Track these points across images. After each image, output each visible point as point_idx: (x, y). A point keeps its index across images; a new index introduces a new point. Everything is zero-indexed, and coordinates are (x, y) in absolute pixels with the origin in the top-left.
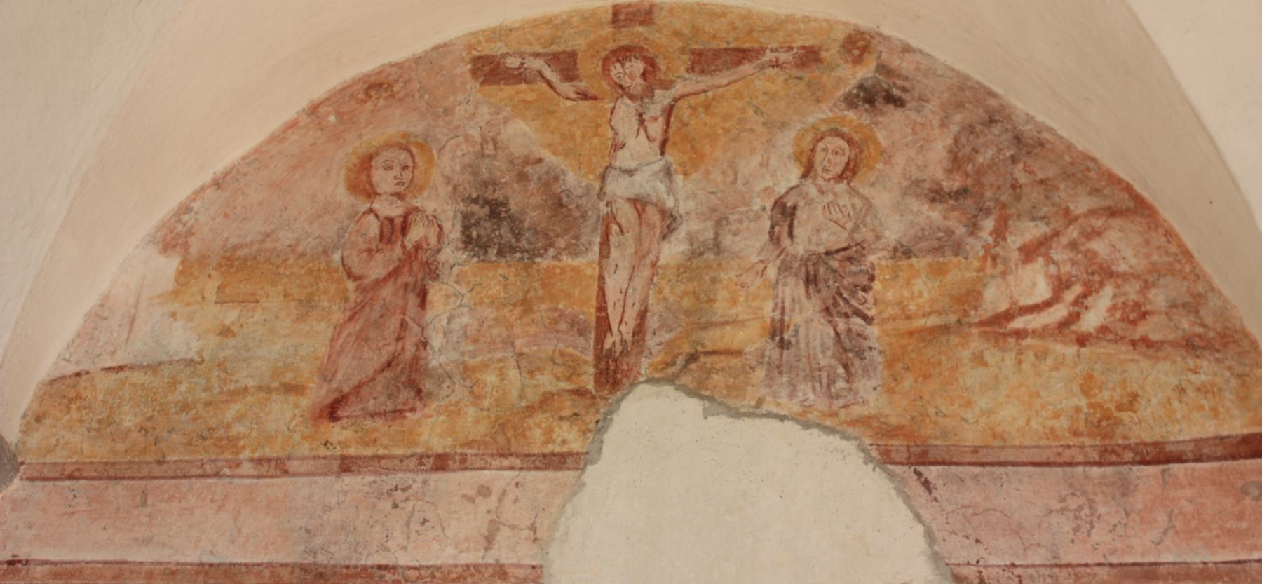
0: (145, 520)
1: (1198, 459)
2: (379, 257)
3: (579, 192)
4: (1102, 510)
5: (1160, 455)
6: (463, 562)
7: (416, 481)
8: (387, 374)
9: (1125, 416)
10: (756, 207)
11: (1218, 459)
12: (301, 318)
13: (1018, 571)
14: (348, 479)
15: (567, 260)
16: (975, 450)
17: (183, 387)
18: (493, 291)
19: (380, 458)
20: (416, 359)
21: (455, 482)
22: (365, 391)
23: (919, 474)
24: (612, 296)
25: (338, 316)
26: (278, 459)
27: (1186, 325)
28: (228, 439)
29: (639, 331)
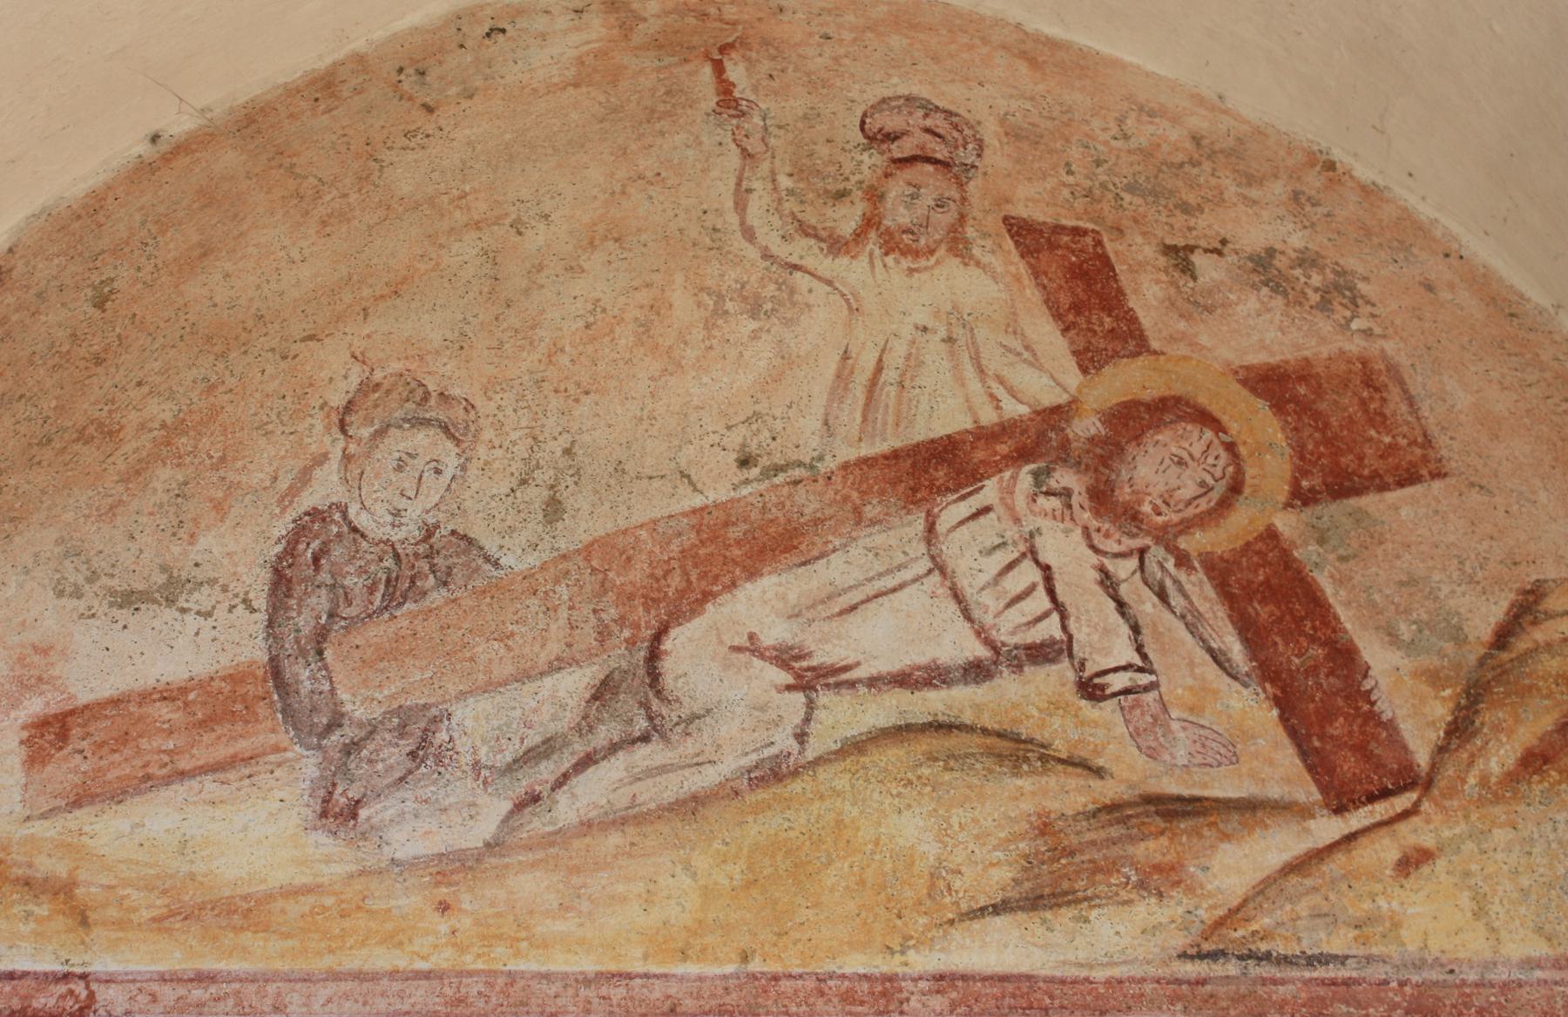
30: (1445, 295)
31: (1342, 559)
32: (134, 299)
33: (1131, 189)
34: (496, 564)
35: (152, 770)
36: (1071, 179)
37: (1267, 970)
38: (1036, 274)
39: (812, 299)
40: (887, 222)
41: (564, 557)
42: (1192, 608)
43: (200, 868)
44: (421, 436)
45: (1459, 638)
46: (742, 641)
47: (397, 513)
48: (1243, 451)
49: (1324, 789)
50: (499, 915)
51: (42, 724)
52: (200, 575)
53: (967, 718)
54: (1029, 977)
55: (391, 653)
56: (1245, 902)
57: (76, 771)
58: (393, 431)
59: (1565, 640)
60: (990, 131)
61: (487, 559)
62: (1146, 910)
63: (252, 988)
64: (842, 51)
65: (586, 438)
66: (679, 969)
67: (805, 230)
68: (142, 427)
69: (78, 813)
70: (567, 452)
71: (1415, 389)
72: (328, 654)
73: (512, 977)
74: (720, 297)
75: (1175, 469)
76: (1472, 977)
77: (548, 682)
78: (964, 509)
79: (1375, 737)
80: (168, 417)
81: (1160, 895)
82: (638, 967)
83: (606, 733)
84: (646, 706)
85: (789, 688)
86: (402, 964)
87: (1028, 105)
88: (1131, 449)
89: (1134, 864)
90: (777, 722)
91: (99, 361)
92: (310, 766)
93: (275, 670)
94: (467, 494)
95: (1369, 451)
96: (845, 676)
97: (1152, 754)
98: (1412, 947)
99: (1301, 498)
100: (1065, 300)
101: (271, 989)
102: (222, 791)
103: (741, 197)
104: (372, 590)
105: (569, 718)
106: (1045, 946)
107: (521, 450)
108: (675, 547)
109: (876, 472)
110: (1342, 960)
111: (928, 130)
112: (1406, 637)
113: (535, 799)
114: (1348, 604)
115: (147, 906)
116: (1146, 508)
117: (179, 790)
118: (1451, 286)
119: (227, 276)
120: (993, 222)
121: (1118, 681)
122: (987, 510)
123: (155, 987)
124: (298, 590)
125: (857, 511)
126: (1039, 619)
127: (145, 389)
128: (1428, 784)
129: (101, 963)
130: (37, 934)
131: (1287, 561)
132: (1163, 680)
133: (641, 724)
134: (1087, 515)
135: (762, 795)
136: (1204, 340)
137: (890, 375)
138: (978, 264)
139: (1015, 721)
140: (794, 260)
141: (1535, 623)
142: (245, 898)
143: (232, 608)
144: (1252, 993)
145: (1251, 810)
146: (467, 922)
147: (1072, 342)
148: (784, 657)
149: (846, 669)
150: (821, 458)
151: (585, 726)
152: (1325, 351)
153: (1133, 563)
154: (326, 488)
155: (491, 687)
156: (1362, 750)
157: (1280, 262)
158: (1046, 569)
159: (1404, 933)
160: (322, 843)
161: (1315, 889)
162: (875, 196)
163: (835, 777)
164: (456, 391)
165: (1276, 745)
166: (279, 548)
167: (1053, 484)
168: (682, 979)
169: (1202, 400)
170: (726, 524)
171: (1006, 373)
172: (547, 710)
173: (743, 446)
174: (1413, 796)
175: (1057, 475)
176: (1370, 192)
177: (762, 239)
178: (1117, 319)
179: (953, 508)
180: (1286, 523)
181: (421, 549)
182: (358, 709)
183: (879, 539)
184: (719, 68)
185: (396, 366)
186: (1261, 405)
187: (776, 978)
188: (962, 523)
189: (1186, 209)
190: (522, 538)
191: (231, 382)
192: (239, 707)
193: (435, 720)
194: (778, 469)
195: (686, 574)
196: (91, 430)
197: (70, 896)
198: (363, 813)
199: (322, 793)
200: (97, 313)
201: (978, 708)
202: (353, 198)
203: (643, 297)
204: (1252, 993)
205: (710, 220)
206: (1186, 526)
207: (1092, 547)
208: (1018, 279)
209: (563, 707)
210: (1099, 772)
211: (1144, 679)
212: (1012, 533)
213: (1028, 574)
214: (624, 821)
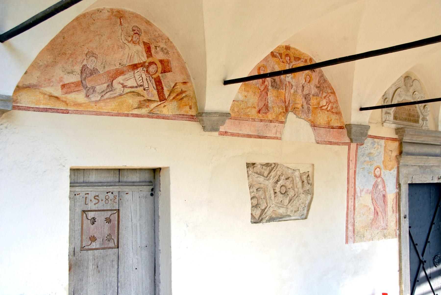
0: (240, 127)
1: (336, 129)
2: (262, 86)
3: (283, 79)
4: (328, 134)
5: (333, 128)
6: (274, 136)
7: (268, 123)
8: (265, 107)
9: (330, 122)
10: (301, 86)
11: (337, 129)
12: (254, 96)
13: (321, 142)
14: (262, 123)
15: (282, 90)
16: (319, 125)
17: (242, 105)
18: (274, 95)
19: (265, 120)
20: (267, 104)
21: (272, 124)
22: (262, 109)
23: (314, 128)
24: (286, 97)
25: (258, 96)
26: (254, 119)
27: (336, 110)
28: (248, 115)
29: (289, 103)
30: (175, 54)
31: (164, 79)
32: (67, 39)
33: (153, 39)
34: (99, 72)
35: (72, 91)
36: (148, 37)
37: (154, 115)
38: (145, 47)
39: (126, 47)
40: (133, 40)
41: (105, 72)
42: (152, 83)
43: (76, 100)
44: (93, 58)
45: (171, 87)
46: (119, 82)
47: (91, 66)
48: (158, 68)
49: (159, 100)
50: (100, 106)
51: (62, 85)
52: (75, 71)
53: (135, 91)
54: (138, 114)
55: (91, 81)
56: (153, 109)
57: (65, 90)
58: (91, 57)
59: (3, 112)
60: (143, 31)
61: (99, 72)
62: (146, 109)
63: (81, 112)
64: (131, 19)
65: (107, 60)
66: (113, 112)
67: (126, 40)
68: (68, 54)
69: (66, 94)
70: (105, 61)
71: (171, 63)
72: (86, 80)
73: (101, 112)
74: (119, 46)
75: (153, 69)
76: (167, 116)
77: (104, 85)
78: (137, 71)
79: (164, 95)
80: (71, 53)
81: (147, 108)
82: (110, 112)
83: (108, 90)
84: (111, 88)
85: (122, 87)
86: (92, 110)
87: (146, 29)
88: (150, 67)
89: (146, 105)
90: (121, 90)
91: (64, 45)
92: (85, 92)
93: (82, 82)
94: (97, 65)
95: (167, 69)
96: (127, 86)
97: (148, 96)
98: (163, 113)
99: (162, 73)
100: (147, 51)
101: (83, 112)
102: (78, 93)
103: (121, 35)
104: (89, 74)
105: (105, 88)
106: (139, 112)
107: (102, 60)
108: (114, 72)
109: (130, 67)
110: (159, 114)
111: (137, 30)
112: (167, 87)
113: (103, 96)
114: (163, 83)
115: (73, 104)
116: (150, 73)
117: (74, 93)
118: (175, 53)
119: (75, 37)
120: (142, 41)
121: (146, 89)
122: (138, 71)
123: (73, 111)
124: (83, 73)
125: (128, 70)
126: (141, 82)
127: (68, 49)
128: (166, 100)
129: (69, 109)
130: (64, 106)
131: (160, 79)
132: (150, 89)
133: (111, 89)
134: (146, 73)
135: (120, 97)
136: (157, 56)
137: (132, 57)
138: (140, 46)
139: (139, 92)
140: (125, 43)
141: (176, 86)
142: (80, 104)
143: (78, 75)
144: (152, 116)
145: (154, 101)
146: (97, 107)
147: (147, 55)
148: (122, 84)
149: (127, 86)
150: (126, 65)
151: (107, 89)
152: (165, 58)
153: (149, 78)
154: (85, 63)
155: (99, 85)
156: (163, 97)
157: (163, 49)
158: (142, 78)
159: (163, 112)
160: (86, 99)
161: (158, 108)
162: (132, 37)
163: (125, 96)
164: (96, 53)
165: (157, 96)
166: (81, 69)
167: (144, 70)
168: (113, 113)
169: (156, 62)
170: (118, 70)
171: (141, 57)
172: (104, 88)
173: (120, 62)
174: (165, 101)
175: (144, 69)
176: (171, 42)
177: (123, 40)
178: (150, 53)
179: (136, 71)
180: (160, 75)
181: (93, 70)
182: (89, 86)
183: (130, 73)
184: (120, 19)
185: (91, 50)
186: (160, 63)
187: (120, 113)
188: (136, 73)
189: (157, 42)
190: (101, 70)
191: (76, 50)
192: (79, 85)
193: (95, 88)
194: (123, 65)
195: (115, 75)
196: (64, 53)
197: (66, 103)
198: (89, 96)
199: (86, 94)
200: (63, 40)
201: (136, 90)
202: (87, 30)
203: (112, 45)
204: (152, 116)
205: (119, 37)
206: (153, 75)
207: (146, 76)
208: (143, 48)
209: (105, 87)
210: (144, 97)
211: (148, 89)
212: (140, 74)
213: (141, 78)
214: (109, 99)
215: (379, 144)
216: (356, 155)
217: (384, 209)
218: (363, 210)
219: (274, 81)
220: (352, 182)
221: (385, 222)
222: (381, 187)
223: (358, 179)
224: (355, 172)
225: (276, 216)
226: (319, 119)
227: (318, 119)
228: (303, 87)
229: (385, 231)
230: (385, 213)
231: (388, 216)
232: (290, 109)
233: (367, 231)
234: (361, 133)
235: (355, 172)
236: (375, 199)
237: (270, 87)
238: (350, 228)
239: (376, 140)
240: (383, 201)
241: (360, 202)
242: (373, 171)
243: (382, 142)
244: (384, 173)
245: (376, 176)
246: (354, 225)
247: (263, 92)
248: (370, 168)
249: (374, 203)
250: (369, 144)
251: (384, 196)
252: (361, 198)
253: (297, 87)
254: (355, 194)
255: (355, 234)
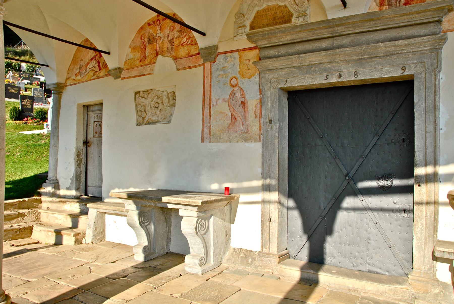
5: (192, 56)
14: (142, 67)
21: (148, 66)
215: (232, 57)
216: (211, 72)
217: (244, 114)
218: (219, 116)
219: (150, 40)
220: (208, 94)
221: (245, 126)
222: (238, 95)
223: (213, 91)
224: (210, 85)
225: (432, 163)
226: (181, 53)
227: (180, 53)
228: (168, 35)
229: (245, 135)
230: (245, 119)
231: (248, 121)
232: (159, 53)
233: (224, 134)
234: (210, 53)
235: (210, 85)
236: (232, 107)
237: (147, 45)
238: (206, 130)
239: (228, 55)
240: (241, 107)
241: (216, 109)
242: (229, 83)
243: (236, 55)
244: (241, 81)
245: (232, 86)
246: (210, 128)
247: (143, 49)
248: (225, 80)
249: (232, 109)
250: (221, 60)
251: (243, 103)
252: (217, 106)
253: (164, 37)
254: (210, 103)
255: (211, 135)
